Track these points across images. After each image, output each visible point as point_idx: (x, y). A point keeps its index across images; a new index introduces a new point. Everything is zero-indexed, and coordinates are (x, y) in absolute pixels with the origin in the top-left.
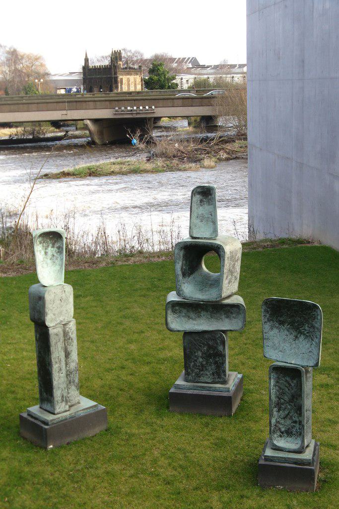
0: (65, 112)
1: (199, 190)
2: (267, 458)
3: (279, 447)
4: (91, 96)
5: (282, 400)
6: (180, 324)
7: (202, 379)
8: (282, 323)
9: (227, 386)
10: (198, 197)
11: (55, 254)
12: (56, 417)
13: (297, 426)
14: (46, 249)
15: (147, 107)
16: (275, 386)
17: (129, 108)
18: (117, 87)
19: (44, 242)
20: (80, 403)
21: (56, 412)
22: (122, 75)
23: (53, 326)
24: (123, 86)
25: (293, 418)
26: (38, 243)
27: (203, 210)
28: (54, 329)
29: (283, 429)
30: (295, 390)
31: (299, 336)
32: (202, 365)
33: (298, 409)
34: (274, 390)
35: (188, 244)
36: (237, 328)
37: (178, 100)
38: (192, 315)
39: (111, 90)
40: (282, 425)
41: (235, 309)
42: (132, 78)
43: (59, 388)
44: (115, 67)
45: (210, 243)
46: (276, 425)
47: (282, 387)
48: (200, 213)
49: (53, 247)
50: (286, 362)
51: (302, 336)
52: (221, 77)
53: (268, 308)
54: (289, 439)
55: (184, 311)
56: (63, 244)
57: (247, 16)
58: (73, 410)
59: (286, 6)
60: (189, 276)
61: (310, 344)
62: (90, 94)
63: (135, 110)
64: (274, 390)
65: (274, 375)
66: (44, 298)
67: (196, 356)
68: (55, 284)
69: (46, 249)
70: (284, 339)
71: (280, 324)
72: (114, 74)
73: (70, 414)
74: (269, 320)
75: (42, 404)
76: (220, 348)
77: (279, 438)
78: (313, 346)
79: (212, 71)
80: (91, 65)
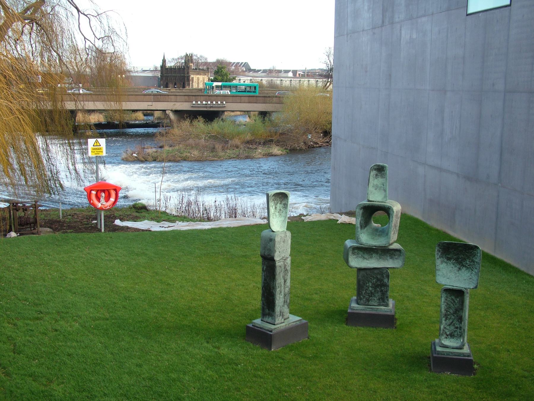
0: (150, 103)
1: (375, 167)
2: (439, 353)
3: (446, 345)
4: (168, 91)
5: (448, 313)
6: (356, 262)
7: (370, 303)
8: (449, 259)
9: (389, 308)
11: (282, 209)
13: (458, 330)
14: (276, 205)
15: (219, 102)
16: (444, 302)
17: (204, 102)
18: (189, 85)
19: (275, 200)
20: (289, 318)
21: (276, 323)
22: (193, 74)
23: (278, 261)
24: (194, 84)
25: (456, 325)
26: (272, 200)
28: (279, 262)
29: (448, 333)
30: (458, 305)
32: (372, 293)
33: (459, 319)
34: (444, 305)
35: (367, 205)
37: (245, 98)
38: (366, 256)
39: (184, 87)
40: (448, 330)
41: (398, 253)
42: (201, 77)
43: (279, 306)
44: (188, 68)
45: (383, 205)
46: (443, 330)
47: (449, 303)
48: (375, 184)
49: (280, 204)
50: (452, 286)
52: (272, 80)
53: (440, 248)
54: (452, 340)
55: (361, 253)
57: (335, 37)
58: (286, 322)
59: (374, 33)
60: (364, 229)
61: (470, 273)
62: (167, 89)
63: (209, 105)
64: (444, 305)
65: (444, 295)
66: (275, 240)
67: (367, 286)
68: (281, 230)
69: (276, 205)
70: (450, 270)
71: (448, 260)
72: (187, 73)
73: (285, 325)
74: (440, 257)
75: (263, 318)
77: (445, 339)
78: (472, 275)
79: (264, 74)
80: (168, 65)
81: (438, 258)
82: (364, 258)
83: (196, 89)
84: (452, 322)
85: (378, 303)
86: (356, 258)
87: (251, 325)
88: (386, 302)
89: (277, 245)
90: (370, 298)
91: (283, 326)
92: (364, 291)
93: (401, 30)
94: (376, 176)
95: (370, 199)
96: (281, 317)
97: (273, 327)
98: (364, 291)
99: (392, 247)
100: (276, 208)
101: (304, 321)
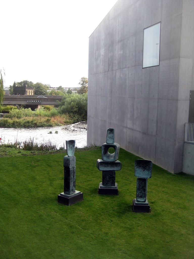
0: (9, 102)
2: (136, 204)
6: (103, 168)
8: (140, 166)
10: (109, 132)
11: (72, 147)
12: (70, 195)
17: (32, 101)
27: (111, 135)
29: (140, 196)
36: (119, 169)
42: (30, 91)
59: (105, 74)
71: (139, 167)
82: (105, 167)
83: (28, 96)
84: (141, 192)
86: (102, 166)
87: (59, 195)
89: (70, 162)
91: (73, 195)
93: (116, 73)
95: (107, 143)
96: (72, 191)
97: (69, 196)
99: (116, 162)
100: (70, 147)
101: (81, 193)
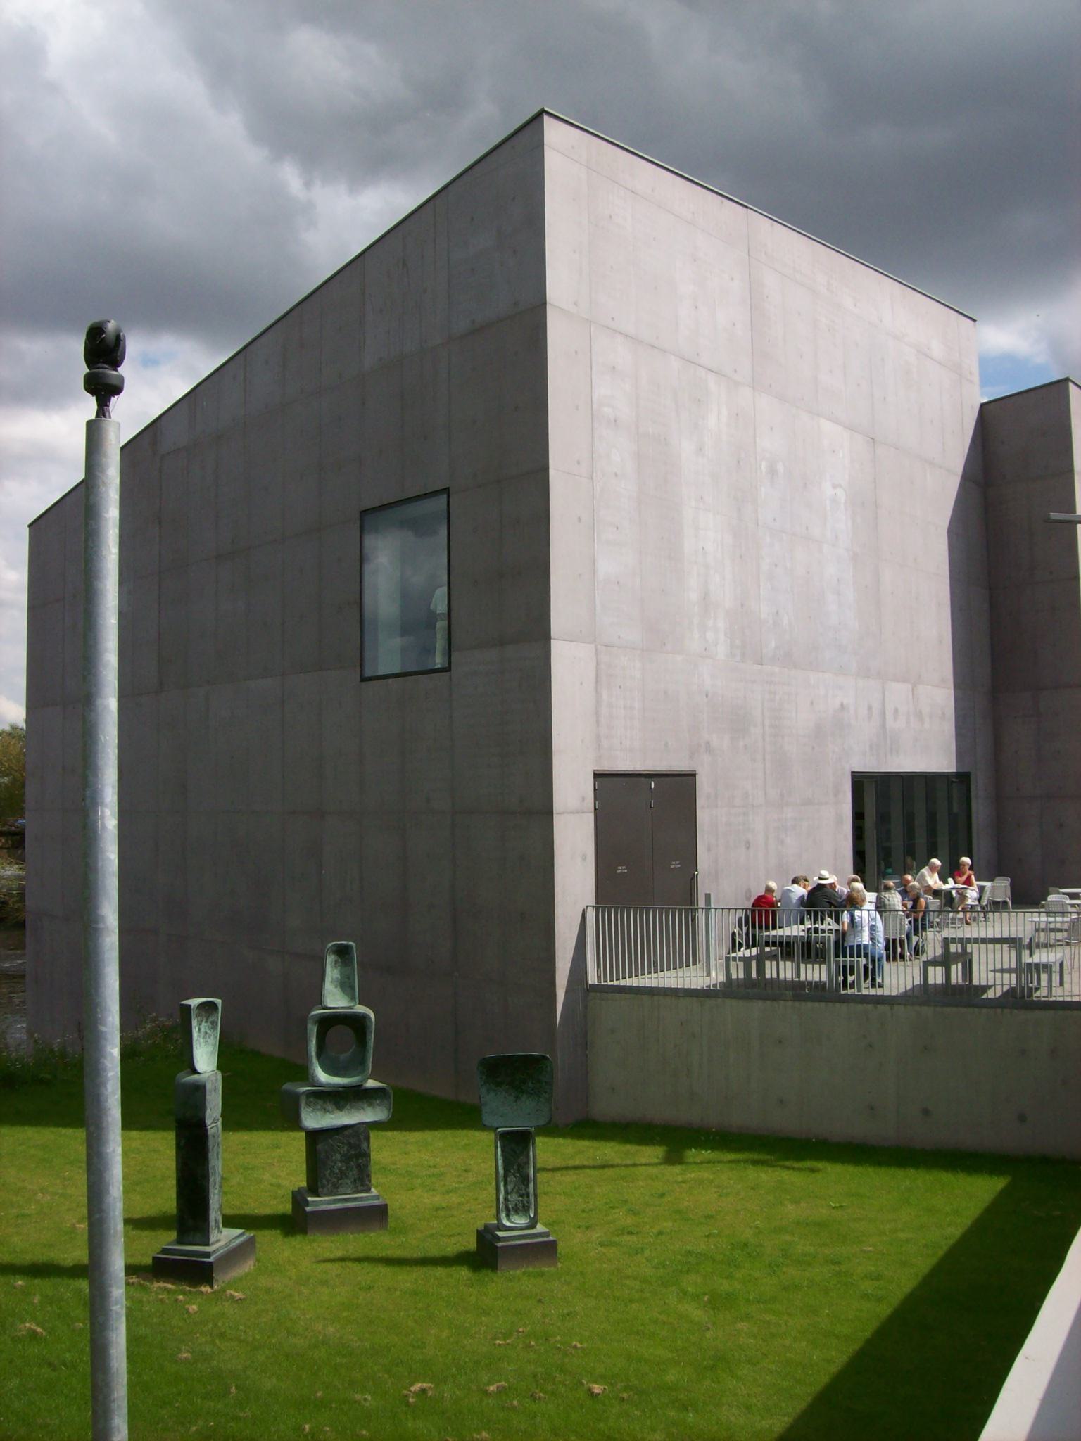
8: (499, 1084)
11: (208, 1031)
31: (520, 1095)
32: (341, 1172)
38: (329, 1106)
49: (206, 1022)
51: (525, 1095)
55: (320, 1102)
56: (218, 1017)
76: (364, 1146)
81: (482, 1086)
82: (326, 1111)
85: (354, 1189)
86: (313, 1111)
88: (367, 1185)
90: (340, 1181)
92: (329, 1171)
94: (336, 964)
98: (329, 1171)
100: (199, 1029)
